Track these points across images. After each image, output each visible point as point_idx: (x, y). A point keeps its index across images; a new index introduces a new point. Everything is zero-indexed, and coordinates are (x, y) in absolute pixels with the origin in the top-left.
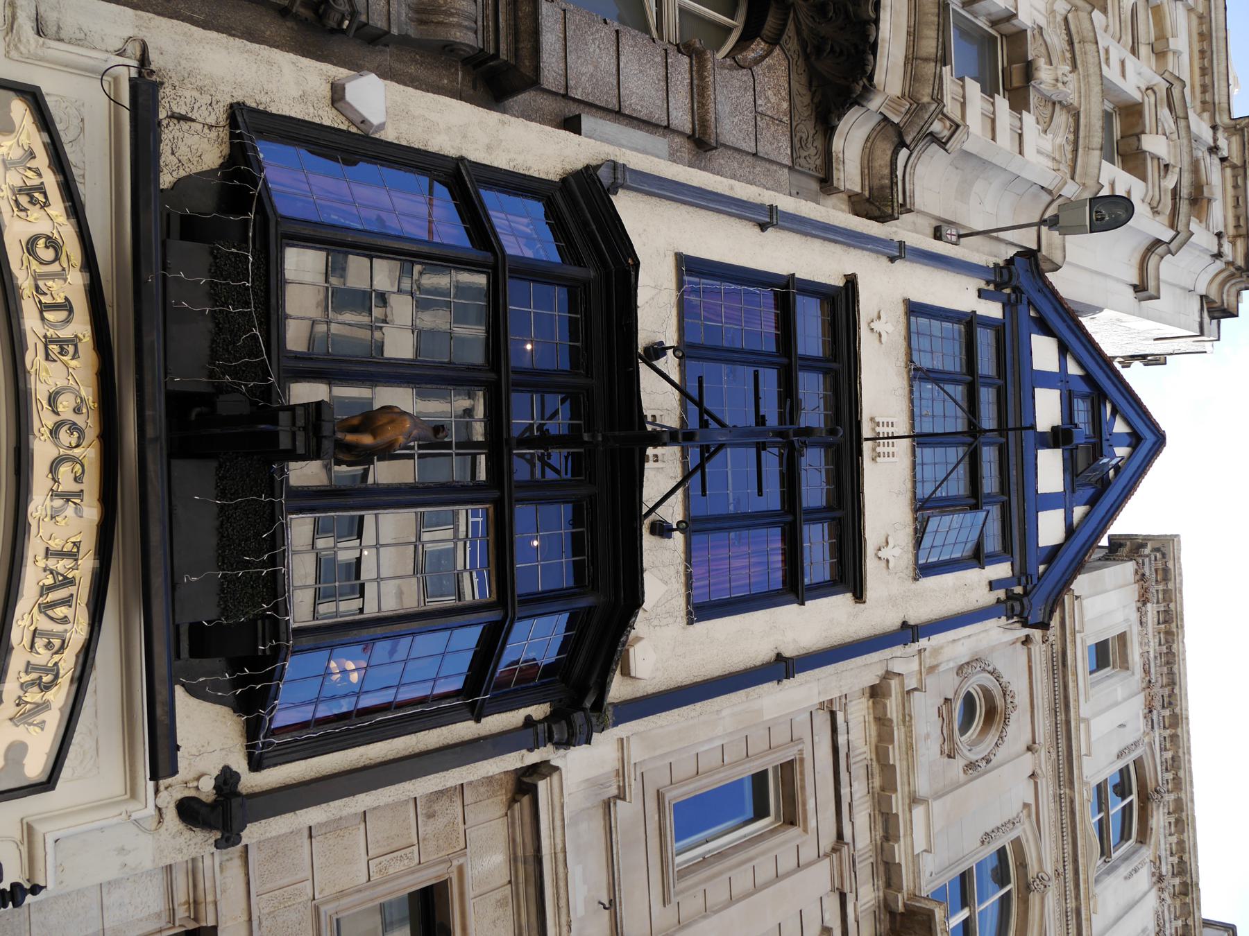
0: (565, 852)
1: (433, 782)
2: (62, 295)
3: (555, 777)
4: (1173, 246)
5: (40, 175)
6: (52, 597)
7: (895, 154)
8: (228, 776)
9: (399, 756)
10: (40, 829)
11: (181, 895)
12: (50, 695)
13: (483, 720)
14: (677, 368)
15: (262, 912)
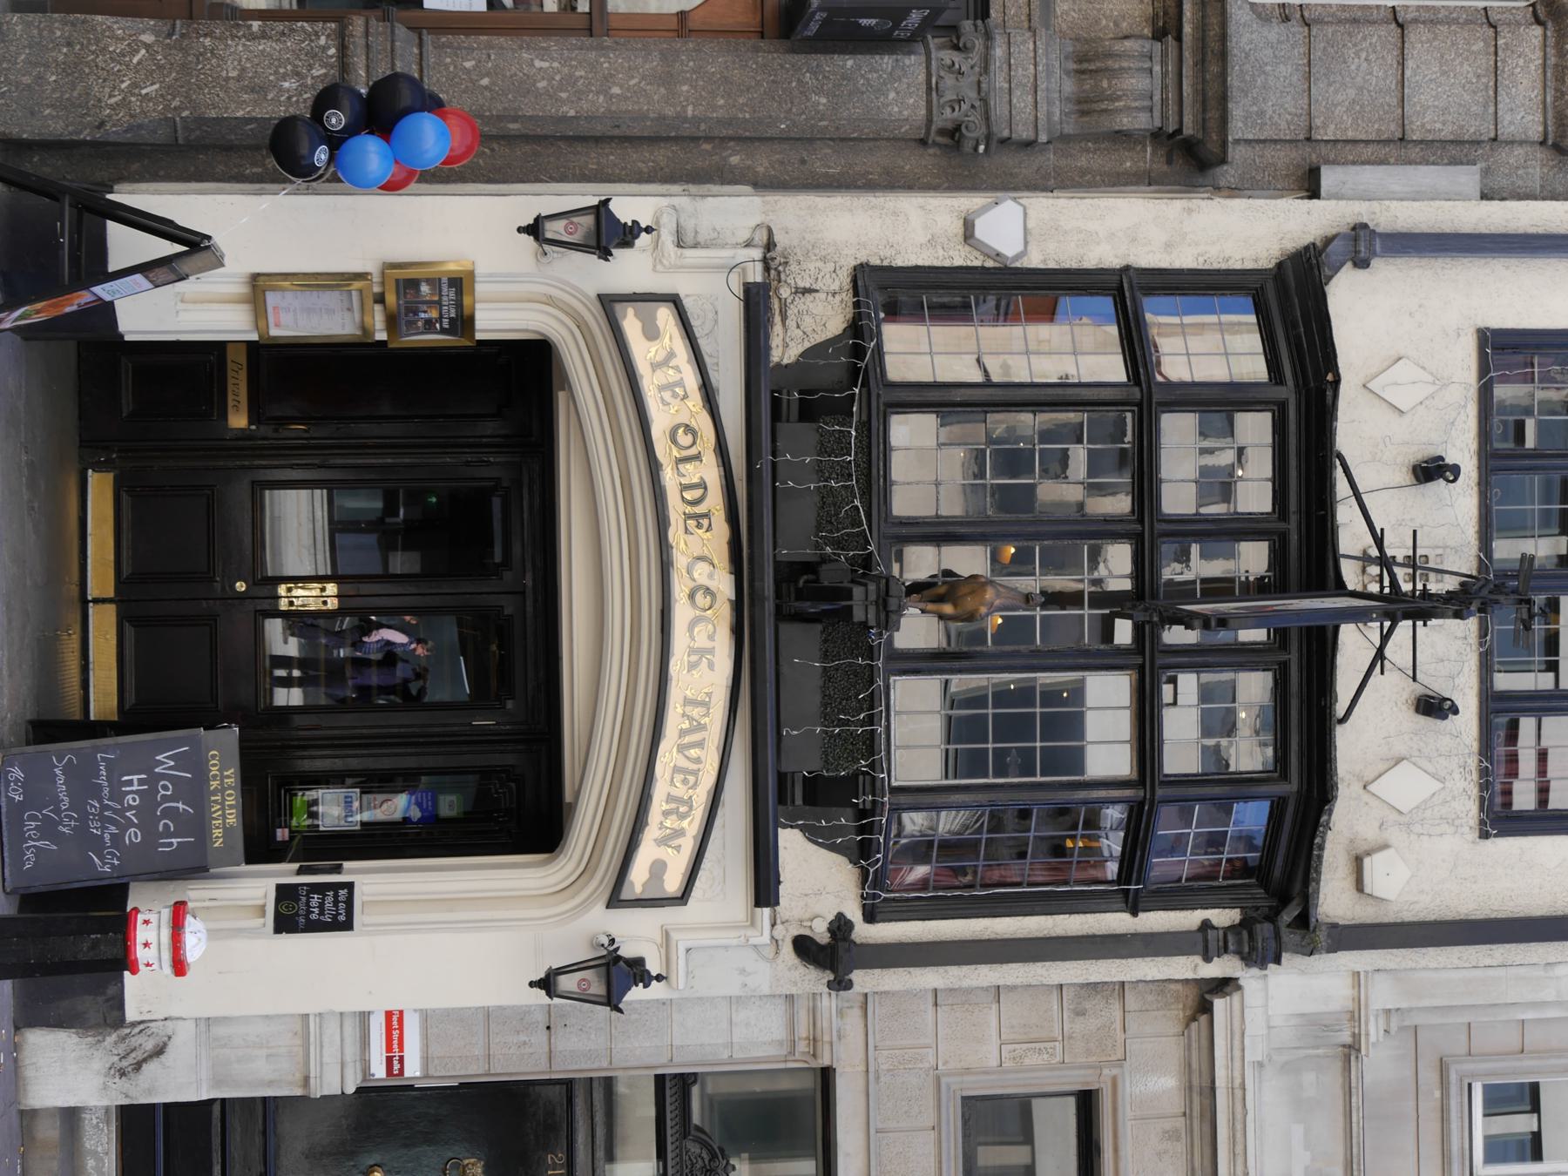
0: (1244, 1089)
1: (1071, 972)
2: (698, 475)
3: (1236, 997)
6: (687, 739)
8: (842, 923)
9: (1030, 936)
10: (674, 936)
11: (803, 1030)
12: (685, 824)
13: (1142, 915)
14: (1476, 489)
15: (882, 1067)
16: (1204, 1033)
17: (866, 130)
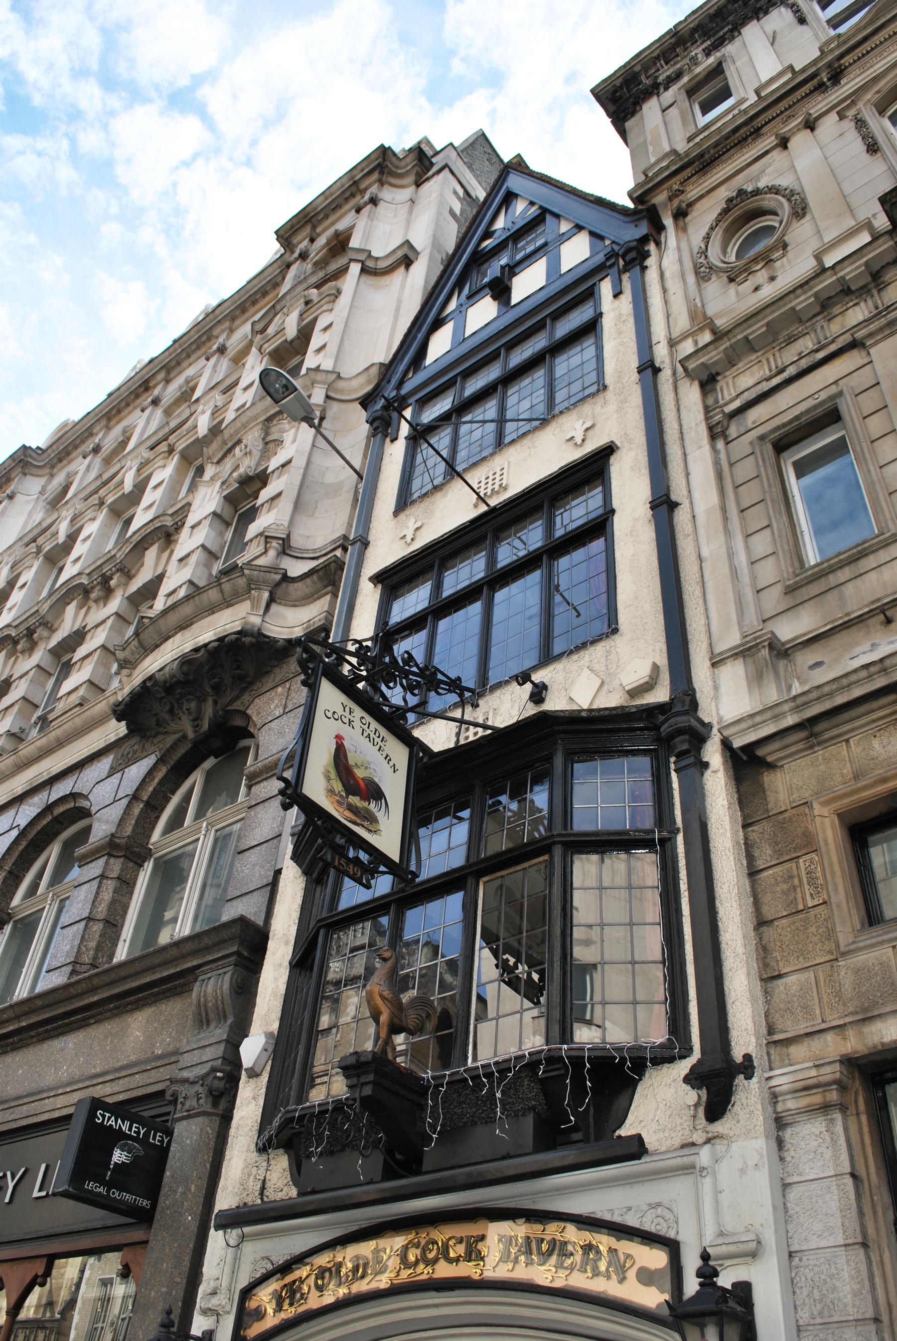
4: (362, 257)
5: (285, 1286)
7: (294, 580)
16: (775, 745)
17: (206, 1158)
